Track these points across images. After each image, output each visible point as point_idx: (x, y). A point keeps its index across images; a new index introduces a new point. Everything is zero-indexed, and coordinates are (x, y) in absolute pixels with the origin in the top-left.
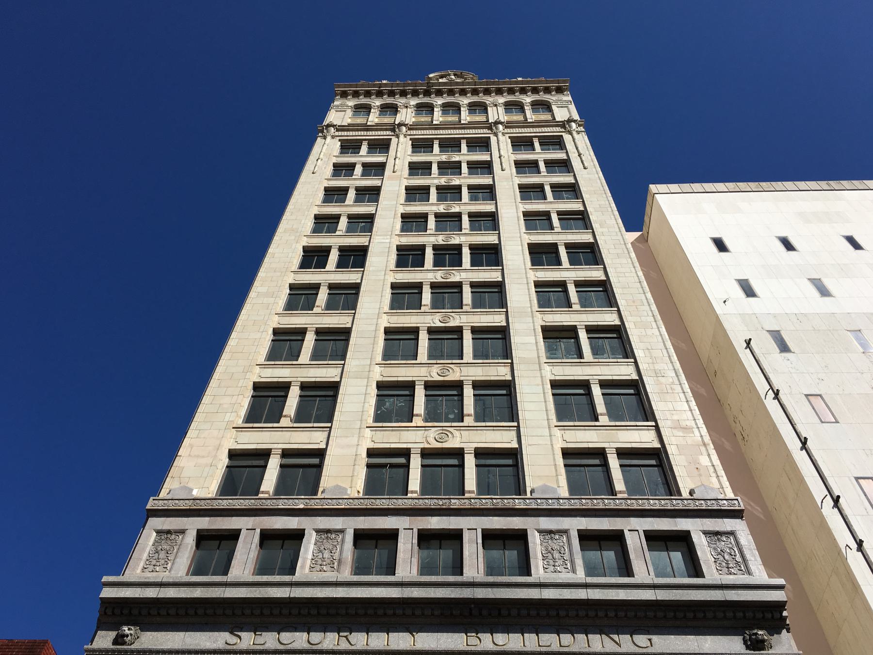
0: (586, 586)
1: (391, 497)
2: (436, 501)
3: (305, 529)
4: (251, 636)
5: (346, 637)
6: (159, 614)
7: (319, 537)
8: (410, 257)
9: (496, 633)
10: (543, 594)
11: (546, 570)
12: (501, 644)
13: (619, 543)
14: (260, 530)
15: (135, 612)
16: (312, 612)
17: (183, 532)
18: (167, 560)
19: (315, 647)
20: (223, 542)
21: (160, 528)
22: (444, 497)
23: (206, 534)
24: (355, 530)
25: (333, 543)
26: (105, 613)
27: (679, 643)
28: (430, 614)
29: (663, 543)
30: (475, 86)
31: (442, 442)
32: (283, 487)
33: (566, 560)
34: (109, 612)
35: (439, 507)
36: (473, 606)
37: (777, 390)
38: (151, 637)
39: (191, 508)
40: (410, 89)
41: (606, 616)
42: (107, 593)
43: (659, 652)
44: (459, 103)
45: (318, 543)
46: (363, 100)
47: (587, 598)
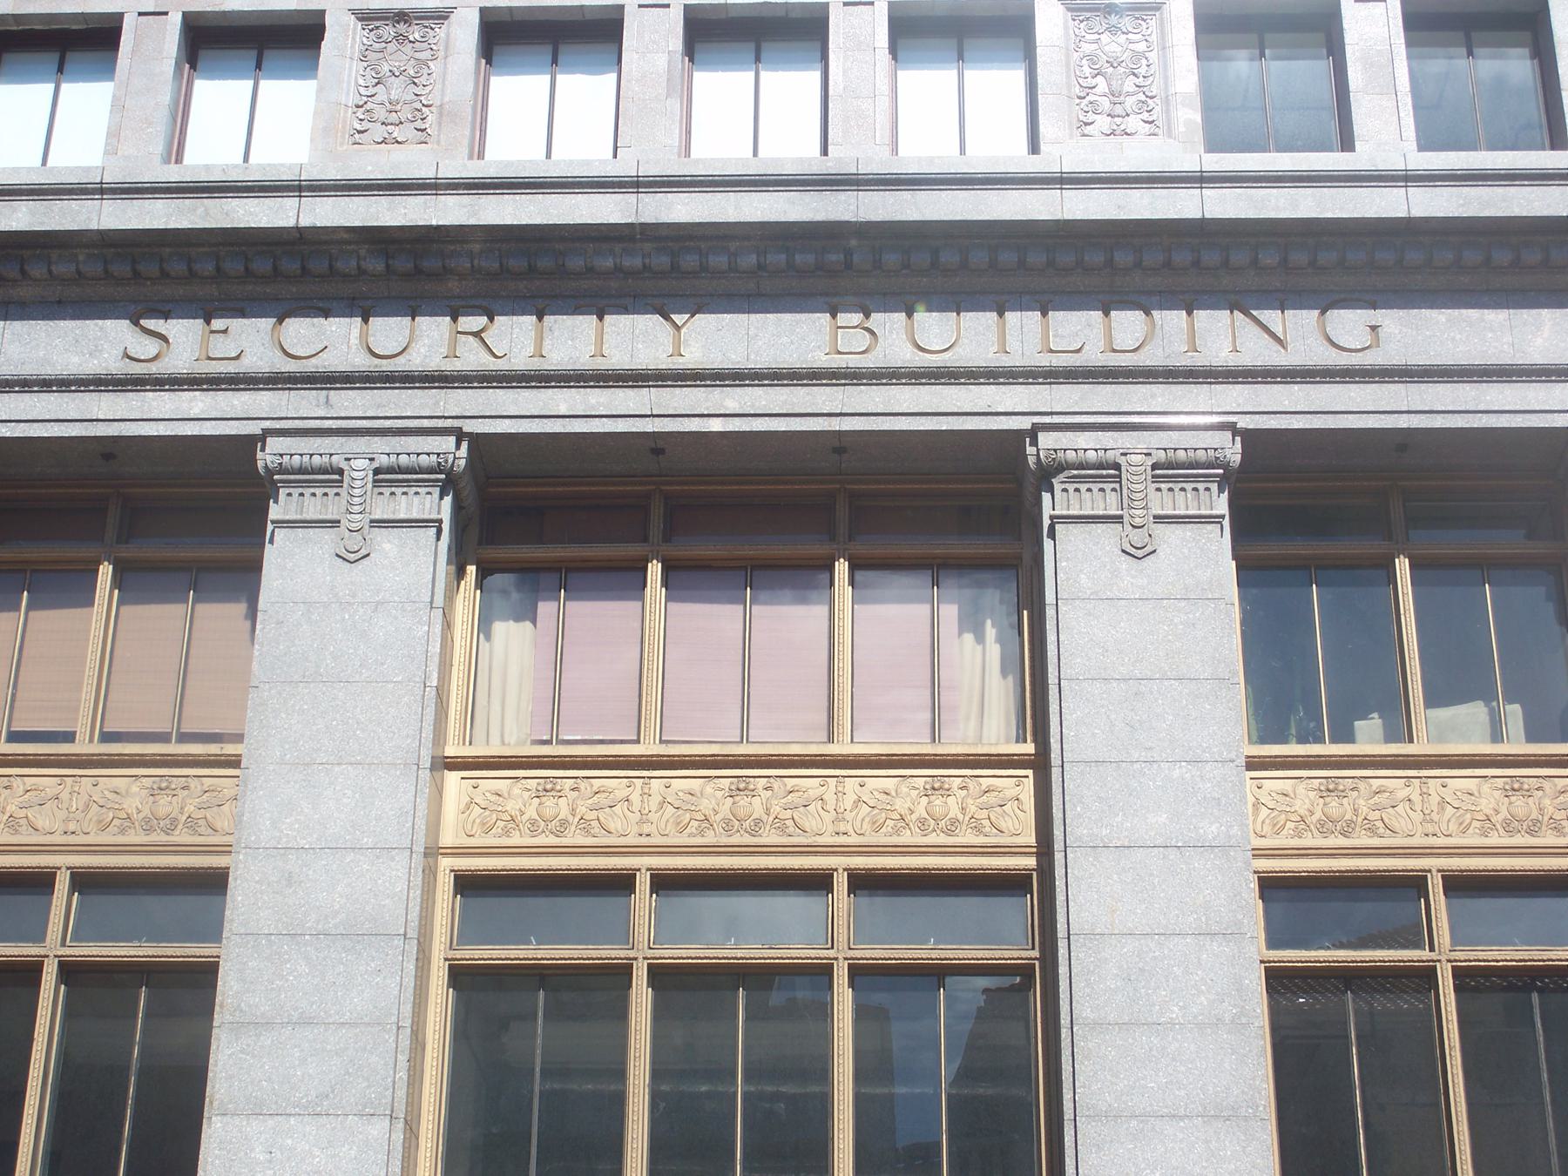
0: (1201, 180)
3: (325, 10)
4: (593, 319)
5: (477, 334)
9: (1198, 309)
10: (1197, 201)
11: (1088, 130)
12: (938, 348)
14: (180, 14)
19: (386, 366)
20: (69, 55)
23: (15, 28)
25: (417, 55)
27: (1458, 337)
28: (725, 267)
29: (953, 42)
33: (1152, 98)
36: (853, 242)
43: (1395, 362)
45: (372, 56)
47: (1199, 216)
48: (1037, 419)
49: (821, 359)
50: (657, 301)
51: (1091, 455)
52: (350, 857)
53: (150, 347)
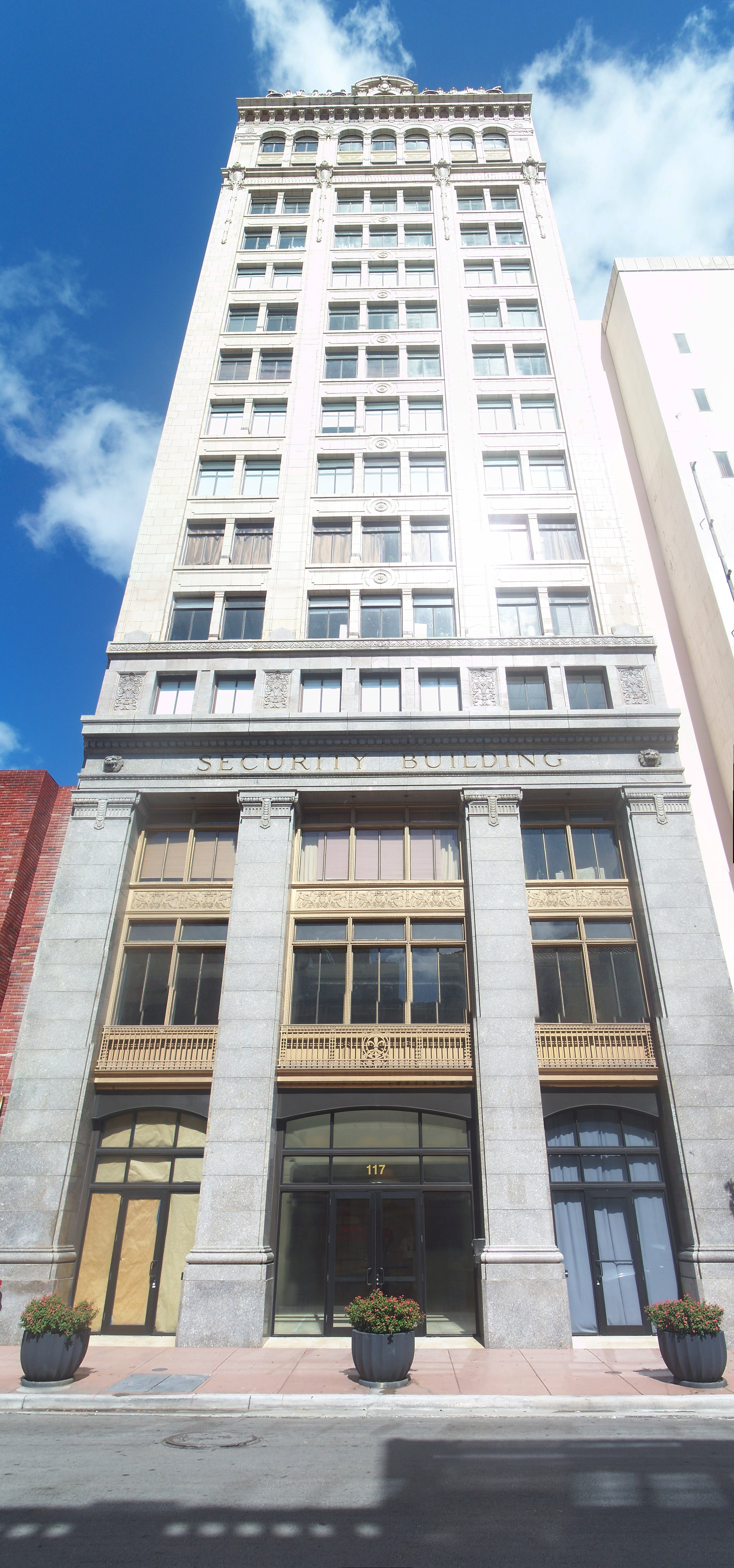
0: (509, 718)
1: (333, 639)
2: (375, 642)
5: (301, 763)
6: (137, 747)
7: (123, 679)
8: (381, 363)
13: (600, 677)
15: (115, 745)
16: (344, 742)
17: (143, 674)
18: (134, 699)
19: (275, 772)
21: (122, 670)
22: (383, 639)
24: (301, 670)
26: (90, 746)
28: (373, 743)
30: (414, 103)
31: (381, 583)
32: (231, 631)
34: (93, 745)
35: (379, 648)
36: (410, 736)
37: (712, 520)
38: (133, 765)
39: (148, 651)
40: (332, 108)
41: (525, 741)
42: (87, 730)
44: (393, 131)
45: (269, 683)
46: (272, 126)
48: (464, 787)
49: (401, 770)
50: (353, 753)
51: (479, 797)
52: (265, 914)
53: (205, 766)
